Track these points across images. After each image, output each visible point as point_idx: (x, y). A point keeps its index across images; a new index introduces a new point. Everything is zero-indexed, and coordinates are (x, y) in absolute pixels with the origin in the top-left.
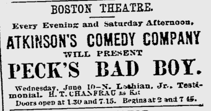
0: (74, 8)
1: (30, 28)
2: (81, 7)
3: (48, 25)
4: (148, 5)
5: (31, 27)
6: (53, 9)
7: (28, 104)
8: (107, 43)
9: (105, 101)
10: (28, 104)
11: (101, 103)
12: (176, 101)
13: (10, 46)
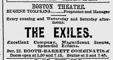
0: (60, 6)
1: (15, 20)
2: (47, 6)
4: (82, 6)
6: (33, 6)
9: (57, 55)
11: (55, 56)
12: (95, 56)
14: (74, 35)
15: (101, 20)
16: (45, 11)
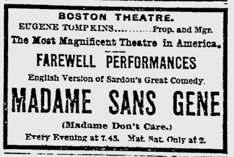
3: (58, 137)
5: (44, 138)
7: (123, 127)
8: (72, 58)
10: (123, 127)
13: (33, 106)
14: (86, 64)
15: (180, 32)
16: (101, 28)
